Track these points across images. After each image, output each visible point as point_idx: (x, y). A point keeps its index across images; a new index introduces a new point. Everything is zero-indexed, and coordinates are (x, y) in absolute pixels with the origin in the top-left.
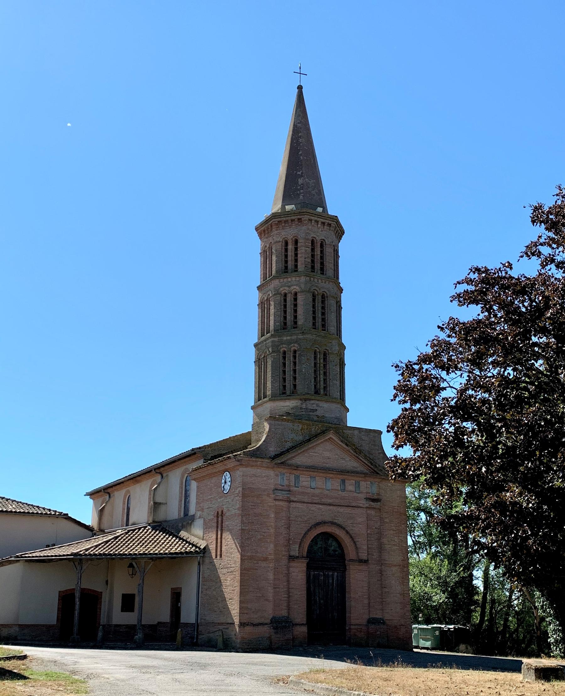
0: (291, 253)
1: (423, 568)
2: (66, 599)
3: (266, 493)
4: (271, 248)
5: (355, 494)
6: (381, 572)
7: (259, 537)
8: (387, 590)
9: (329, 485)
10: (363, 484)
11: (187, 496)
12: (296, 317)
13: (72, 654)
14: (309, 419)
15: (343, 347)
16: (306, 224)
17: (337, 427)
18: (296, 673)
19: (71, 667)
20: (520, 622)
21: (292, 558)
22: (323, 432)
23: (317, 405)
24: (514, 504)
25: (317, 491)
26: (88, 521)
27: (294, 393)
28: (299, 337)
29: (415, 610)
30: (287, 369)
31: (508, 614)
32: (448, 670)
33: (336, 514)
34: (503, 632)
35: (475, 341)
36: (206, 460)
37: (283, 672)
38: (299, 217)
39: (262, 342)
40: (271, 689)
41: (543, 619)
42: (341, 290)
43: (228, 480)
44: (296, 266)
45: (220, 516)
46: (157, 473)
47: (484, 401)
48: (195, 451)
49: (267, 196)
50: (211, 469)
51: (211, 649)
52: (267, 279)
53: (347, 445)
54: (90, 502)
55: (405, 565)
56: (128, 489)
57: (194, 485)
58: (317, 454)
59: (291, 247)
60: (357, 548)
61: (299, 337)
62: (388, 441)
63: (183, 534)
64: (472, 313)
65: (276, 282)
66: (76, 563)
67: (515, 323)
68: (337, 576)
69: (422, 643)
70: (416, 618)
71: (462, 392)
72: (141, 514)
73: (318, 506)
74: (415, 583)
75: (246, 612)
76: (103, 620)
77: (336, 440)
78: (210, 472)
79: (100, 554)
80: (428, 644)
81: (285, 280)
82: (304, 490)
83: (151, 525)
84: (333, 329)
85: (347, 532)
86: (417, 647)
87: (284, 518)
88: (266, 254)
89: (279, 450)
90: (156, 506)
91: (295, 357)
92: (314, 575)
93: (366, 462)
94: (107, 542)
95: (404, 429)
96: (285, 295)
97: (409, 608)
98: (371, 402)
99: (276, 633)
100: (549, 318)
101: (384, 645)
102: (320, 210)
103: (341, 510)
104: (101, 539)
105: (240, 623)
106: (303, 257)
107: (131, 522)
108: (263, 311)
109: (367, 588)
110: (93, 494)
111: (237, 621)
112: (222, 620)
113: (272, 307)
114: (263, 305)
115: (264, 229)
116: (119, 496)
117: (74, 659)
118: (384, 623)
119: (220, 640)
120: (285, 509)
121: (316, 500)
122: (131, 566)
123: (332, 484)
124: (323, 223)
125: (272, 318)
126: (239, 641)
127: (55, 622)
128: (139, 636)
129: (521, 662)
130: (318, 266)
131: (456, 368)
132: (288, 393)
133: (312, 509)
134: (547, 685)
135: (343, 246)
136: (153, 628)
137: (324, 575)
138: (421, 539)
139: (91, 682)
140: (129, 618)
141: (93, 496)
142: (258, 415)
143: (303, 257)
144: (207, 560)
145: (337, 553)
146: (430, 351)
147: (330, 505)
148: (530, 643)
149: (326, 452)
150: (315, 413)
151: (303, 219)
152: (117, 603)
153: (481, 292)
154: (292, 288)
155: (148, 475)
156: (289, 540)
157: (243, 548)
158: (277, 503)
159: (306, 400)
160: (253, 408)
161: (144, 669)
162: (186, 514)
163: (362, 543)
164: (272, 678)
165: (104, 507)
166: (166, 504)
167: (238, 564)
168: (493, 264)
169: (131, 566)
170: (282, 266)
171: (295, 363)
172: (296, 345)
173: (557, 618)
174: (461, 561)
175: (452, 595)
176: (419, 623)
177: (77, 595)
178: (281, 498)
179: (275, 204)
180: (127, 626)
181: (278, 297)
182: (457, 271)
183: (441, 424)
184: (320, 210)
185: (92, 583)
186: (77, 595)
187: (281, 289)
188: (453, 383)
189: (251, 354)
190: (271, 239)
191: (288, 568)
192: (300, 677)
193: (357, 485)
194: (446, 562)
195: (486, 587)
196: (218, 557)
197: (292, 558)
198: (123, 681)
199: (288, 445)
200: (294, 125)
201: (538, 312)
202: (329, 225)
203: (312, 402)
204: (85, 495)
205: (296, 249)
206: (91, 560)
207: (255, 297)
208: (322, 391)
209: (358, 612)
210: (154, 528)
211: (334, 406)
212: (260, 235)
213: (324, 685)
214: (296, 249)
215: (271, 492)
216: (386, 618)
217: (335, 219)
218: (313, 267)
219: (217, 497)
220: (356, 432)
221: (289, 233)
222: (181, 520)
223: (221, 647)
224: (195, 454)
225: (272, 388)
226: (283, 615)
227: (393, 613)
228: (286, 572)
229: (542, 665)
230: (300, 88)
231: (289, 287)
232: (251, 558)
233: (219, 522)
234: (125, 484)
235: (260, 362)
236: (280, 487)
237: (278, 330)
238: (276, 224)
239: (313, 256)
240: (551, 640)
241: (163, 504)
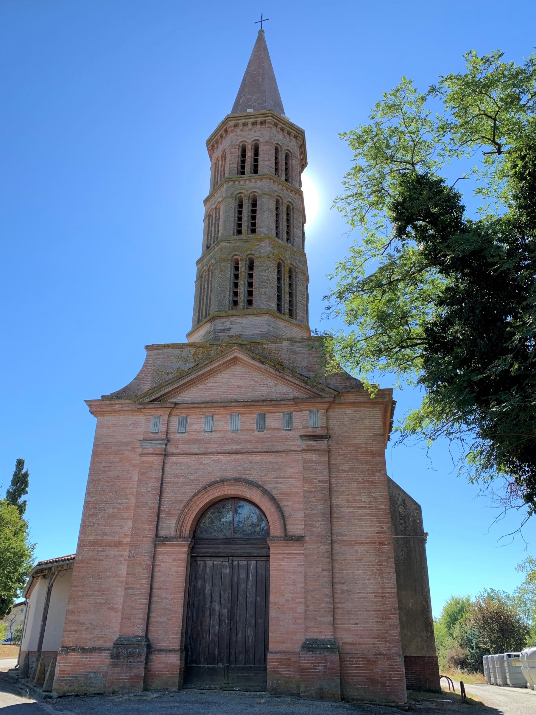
3: (129, 448)
5: (284, 433)
7: (111, 511)
8: (345, 587)
16: (233, 131)
33: (245, 466)
53: (262, 363)
58: (218, 384)
59: (249, 154)
60: (283, 516)
68: (256, 568)
73: (214, 457)
75: (74, 628)
82: (192, 437)
87: (154, 480)
92: (213, 567)
93: (297, 382)
109: (303, 585)
112: (434, 656)
120: (155, 467)
121: (214, 448)
124: (254, 124)
133: (204, 462)
137: (232, 567)
147: (236, 453)
150: (228, 333)
158: (144, 459)
178: (150, 451)
203: (223, 320)
215: (138, 445)
216: (345, 640)
226: (136, 633)
232: (95, 543)
236: (151, 435)
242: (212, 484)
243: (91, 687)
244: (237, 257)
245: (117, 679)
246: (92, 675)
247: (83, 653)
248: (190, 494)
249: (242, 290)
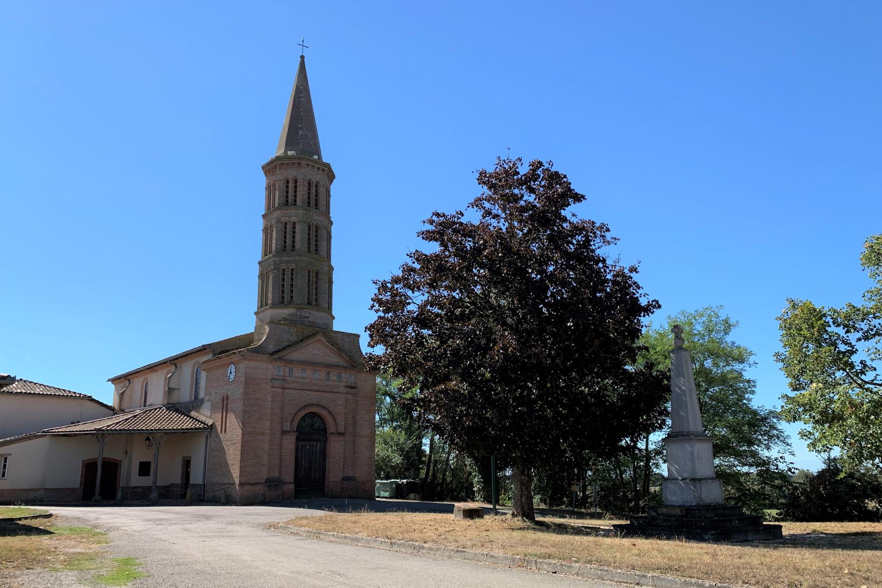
0: (291, 190)
1: (386, 439)
2: (89, 467)
4: (274, 185)
6: (354, 441)
9: (317, 376)
10: (343, 375)
11: (197, 384)
12: (294, 242)
13: (94, 512)
14: (302, 324)
15: (331, 268)
17: (325, 331)
18: (285, 520)
19: (93, 523)
20: (454, 475)
21: (284, 432)
22: (313, 335)
24: (455, 391)
25: (307, 381)
26: (110, 404)
27: (291, 302)
29: (379, 469)
30: (285, 284)
31: (445, 470)
32: (401, 513)
34: (442, 483)
35: (433, 270)
36: (214, 355)
37: (274, 519)
40: (265, 533)
41: (470, 473)
42: (331, 223)
43: (233, 370)
44: (295, 201)
45: (225, 400)
47: (438, 315)
49: (274, 145)
50: (218, 363)
52: (270, 208)
54: (112, 387)
55: (373, 435)
57: (203, 374)
59: (291, 185)
60: (336, 424)
62: (364, 340)
63: (193, 414)
64: (433, 248)
65: (278, 213)
67: (464, 258)
69: (383, 494)
70: (379, 475)
71: (422, 308)
72: (157, 396)
74: (380, 450)
76: (122, 483)
79: (120, 430)
80: (387, 494)
84: (324, 254)
85: (330, 412)
86: (378, 497)
88: (270, 189)
89: (277, 348)
90: (170, 391)
91: (292, 274)
94: (127, 420)
95: (377, 332)
96: (286, 224)
97: (374, 468)
98: (352, 312)
100: (486, 256)
101: (353, 497)
102: (316, 157)
103: (325, 395)
104: (122, 417)
106: (300, 193)
107: (148, 403)
108: (266, 236)
110: (114, 380)
111: (237, 481)
112: (225, 481)
113: (274, 233)
114: (267, 231)
115: (270, 168)
116: (138, 383)
117: (95, 515)
118: (354, 480)
119: (223, 497)
122: (148, 439)
123: (320, 375)
124: (318, 168)
125: (274, 241)
127: (78, 486)
128: (154, 495)
129: (453, 506)
130: (313, 202)
131: (419, 289)
132: (286, 303)
134: (471, 522)
135: (334, 188)
136: (167, 488)
138: (387, 417)
139: (111, 535)
140: (146, 481)
142: (260, 320)
143: (300, 193)
144: (213, 434)
146: (400, 274)
148: (461, 491)
149: (315, 350)
152: (135, 468)
153: (439, 233)
156: (282, 418)
157: (244, 424)
159: (300, 309)
160: (256, 313)
161: (158, 521)
162: (196, 397)
163: (341, 420)
164: (264, 524)
167: (240, 437)
168: (450, 212)
169: (148, 439)
170: (283, 199)
171: (292, 279)
173: (480, 472)
174: (414, 431)
175: (406, 456)
176: (381, 479)
179: (279, 149)
180: (144, 488)
181: (280, 225)
182: (419, 221)
183: (405, 330)
184: (316, 157)
185: (112, 453)
186: (100, 464)
188: (417, 299)
189: (256, 270)
190: (274, 178)
191: (281, 440)
192: (288, 523)
193: (339, 376)
194: (404, 433)
195: (431, 452)
197: (284, 432)
198: (139, 532)
199: (285, 344)
201: (478, 251)
202: (324, 170)
205: (296, 187)
206: (113, 434)
207: (260, 224)
208: (314, 303)
209: (335, 473)
210: (168, 409)
211: (323, 314)
212: (266, 173)
213: (307, 529)
214: (296, 187)
217: (328, 166)
218: (309, 203)
220: (340, 335)
221: (291, 173)
222: (191, 402)
227: (361, 472)
229: (468, 508)
230: (302, 57)
233: (224, 405)
235: (263, 276)
239: (309, 194)
240: (475, 489)
242: (306, 406)
248: (296, 410)
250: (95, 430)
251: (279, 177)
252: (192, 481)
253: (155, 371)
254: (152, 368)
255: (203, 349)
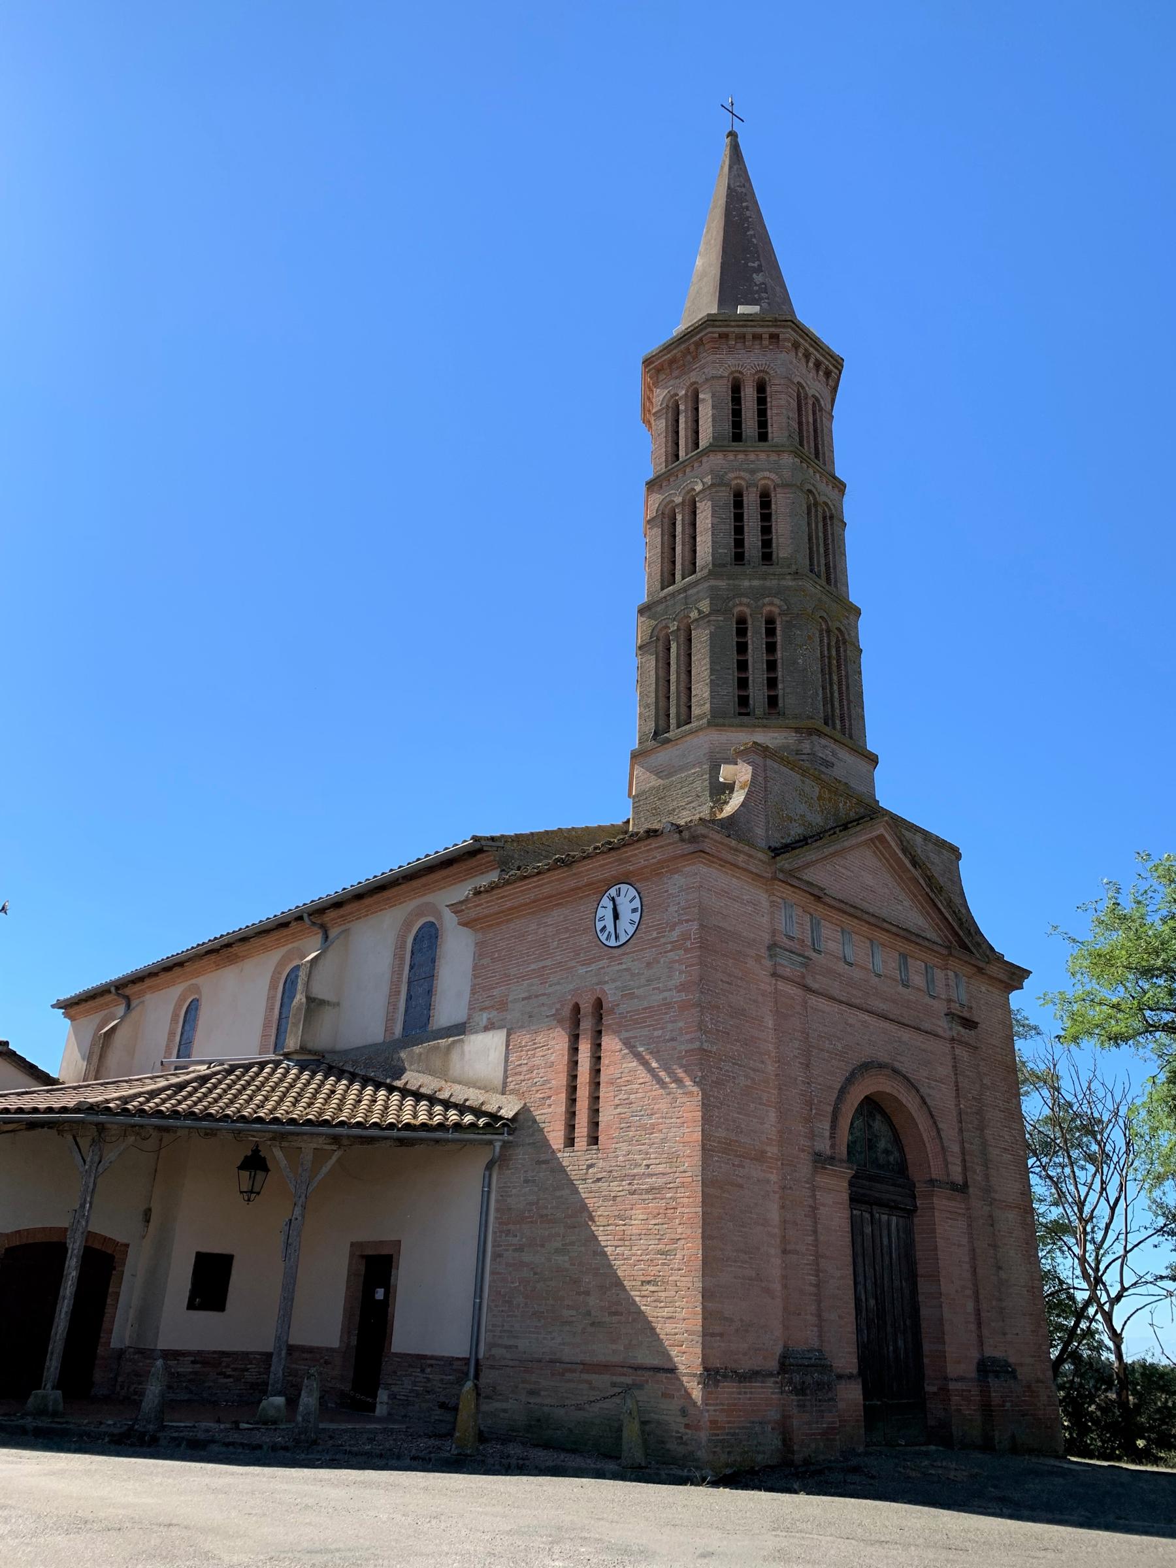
23: (834, 754)
28: (784, 583)
38: (772, 330)
39: (660, 602)
46: (314, 924)
48: (483, 843)
51: (590, 1463)
54: (62, 1024)
56: (193, 981)
58: (849, 873)
59: (749, 394)
61: (784, 583)
66: (84, 1143)
77: (893, 844)
78: (546, 890)
81: (741, 456)
83: (296, 1057)
93: (954, 924)
99: (801, 1406)
105: (706, 1369)
110: (71, 1006)
112: (603, 1350)
116: (159, 1010)
126: (703, 1436)
127: (335, 1343)
133: (850, 1021)
141: (72, 1011)
144: (522, 1156)
145: (891, 1159)
151: (781, 336)
152: (180, 1277)
154: (760, 475)
155: (275, 935)
165: (114, 1029)
166: (338, 1004)
172: (777, 601)
177: (75, 1248)
186: (75, 1248)
187: (731, 475)
190: (693, 377)
196: (581, 1142)
199: (796, 831)
200: (729, 188)
203: (823, 741)
204: (53, 1006)
215: (764, 952)
219: (573, 963)
223: (639, 1456)
224: (480, 851)
225: (712, 697)
228: (810, 1202)
230: (732, 135)
231: (753, 472)
234: (189, 968)
237: (724, 566)
238: (713, 340)
241: (328, 1003)
243: (758, 1453)
244: (773, 609)
245: (807, 1435)
246: (757, 1429)
247: (740, 1382)
249: (757, 674)
250: (77, 1109)
251: (710, 371)
252: (405, 1337)
253: (233, 960)
254: (223, 951)
255: (475, 853)
